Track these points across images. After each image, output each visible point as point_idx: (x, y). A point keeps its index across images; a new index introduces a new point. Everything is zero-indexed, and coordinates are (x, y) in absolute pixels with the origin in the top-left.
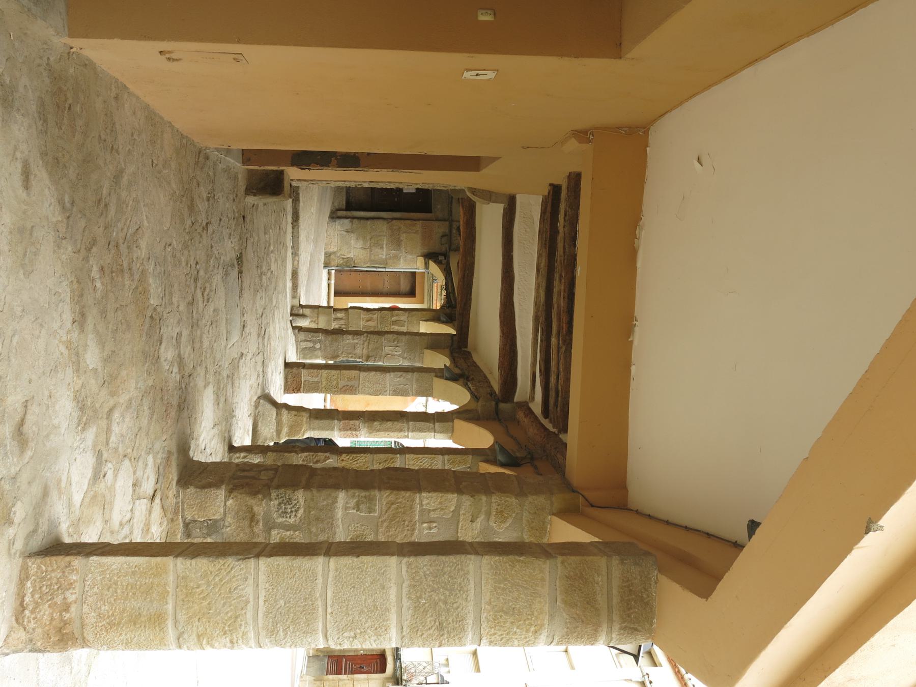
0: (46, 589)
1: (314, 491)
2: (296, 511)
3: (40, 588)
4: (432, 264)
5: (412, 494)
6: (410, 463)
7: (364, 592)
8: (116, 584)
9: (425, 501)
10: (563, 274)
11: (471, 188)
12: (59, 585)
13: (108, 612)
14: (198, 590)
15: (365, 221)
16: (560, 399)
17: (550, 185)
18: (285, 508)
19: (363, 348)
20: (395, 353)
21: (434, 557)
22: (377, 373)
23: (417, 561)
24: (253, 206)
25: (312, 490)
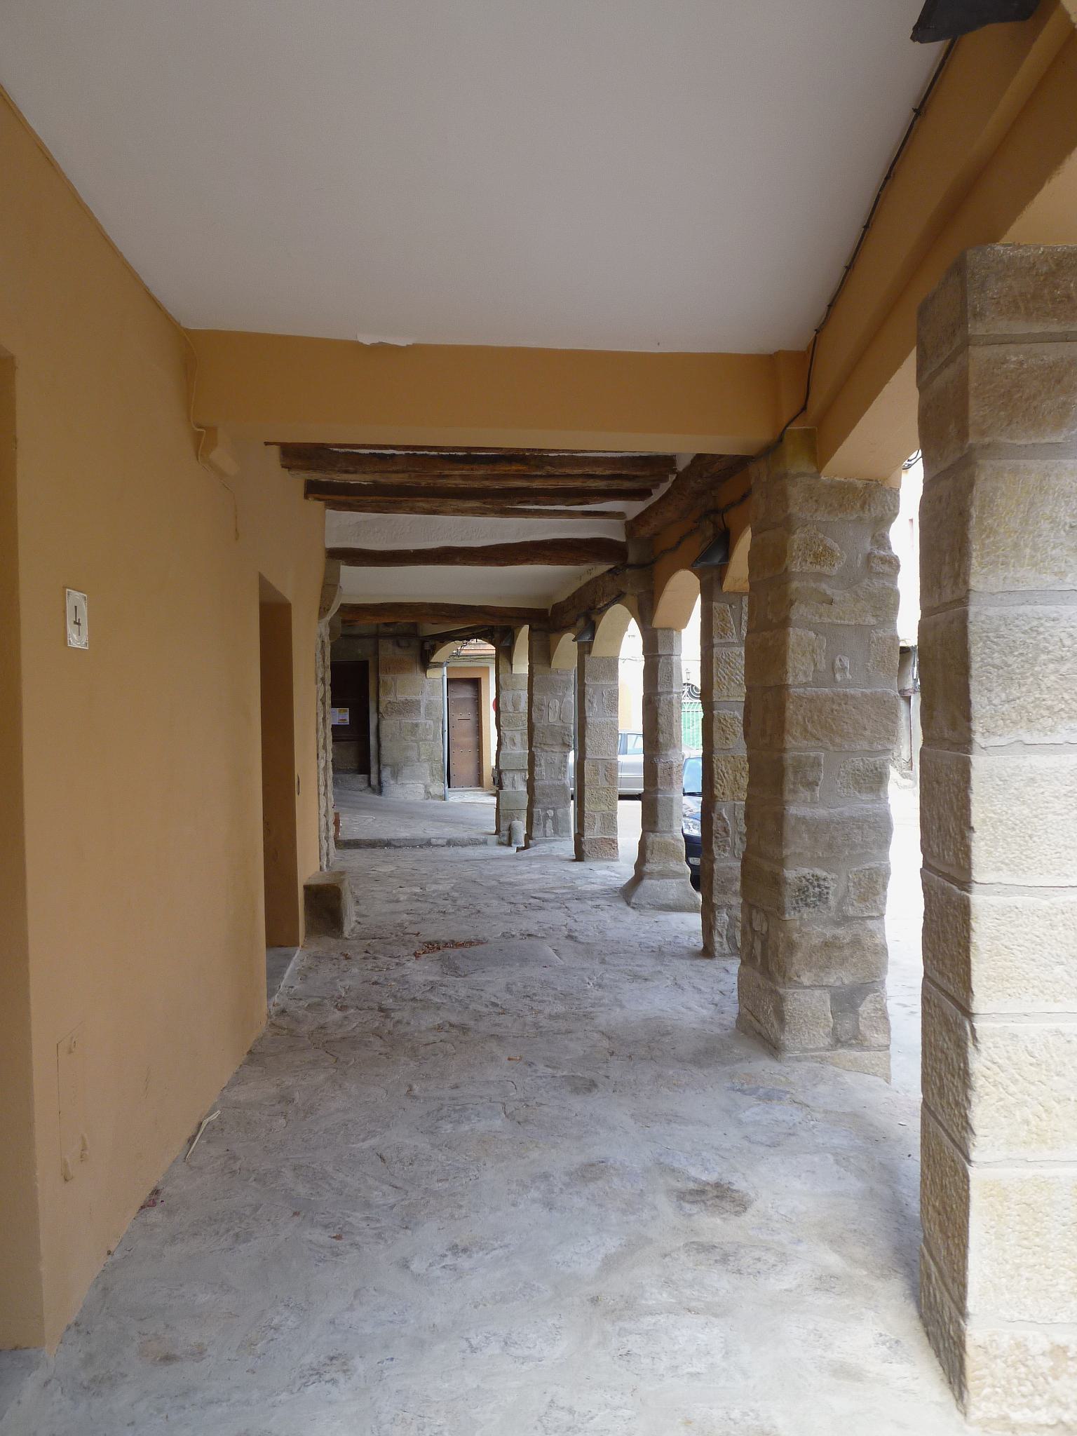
0: (1025, 1386)
1: (786, 852)
2: (818, 879)
3: (1024, 1396)
4: (435, 659)
5: (791, 700)
6: (726, 694)
7: (1041, 816)
8: (1018, 1267)
9: (801, 678)
10: (437, 472)
11: (319, 614)
12: (1019, 1365)
13: (1071, 1278)
14: (1033, 1122)
15: (383, 748)
16: (624, 472)
17: (306, 497)
18: (814, 896)
19: (552, 751)
20: (557, 707)
21: (974, 686)
22: (586, 735)
23: (982, 717)
24: (359, 923)
25: (787, 856)
